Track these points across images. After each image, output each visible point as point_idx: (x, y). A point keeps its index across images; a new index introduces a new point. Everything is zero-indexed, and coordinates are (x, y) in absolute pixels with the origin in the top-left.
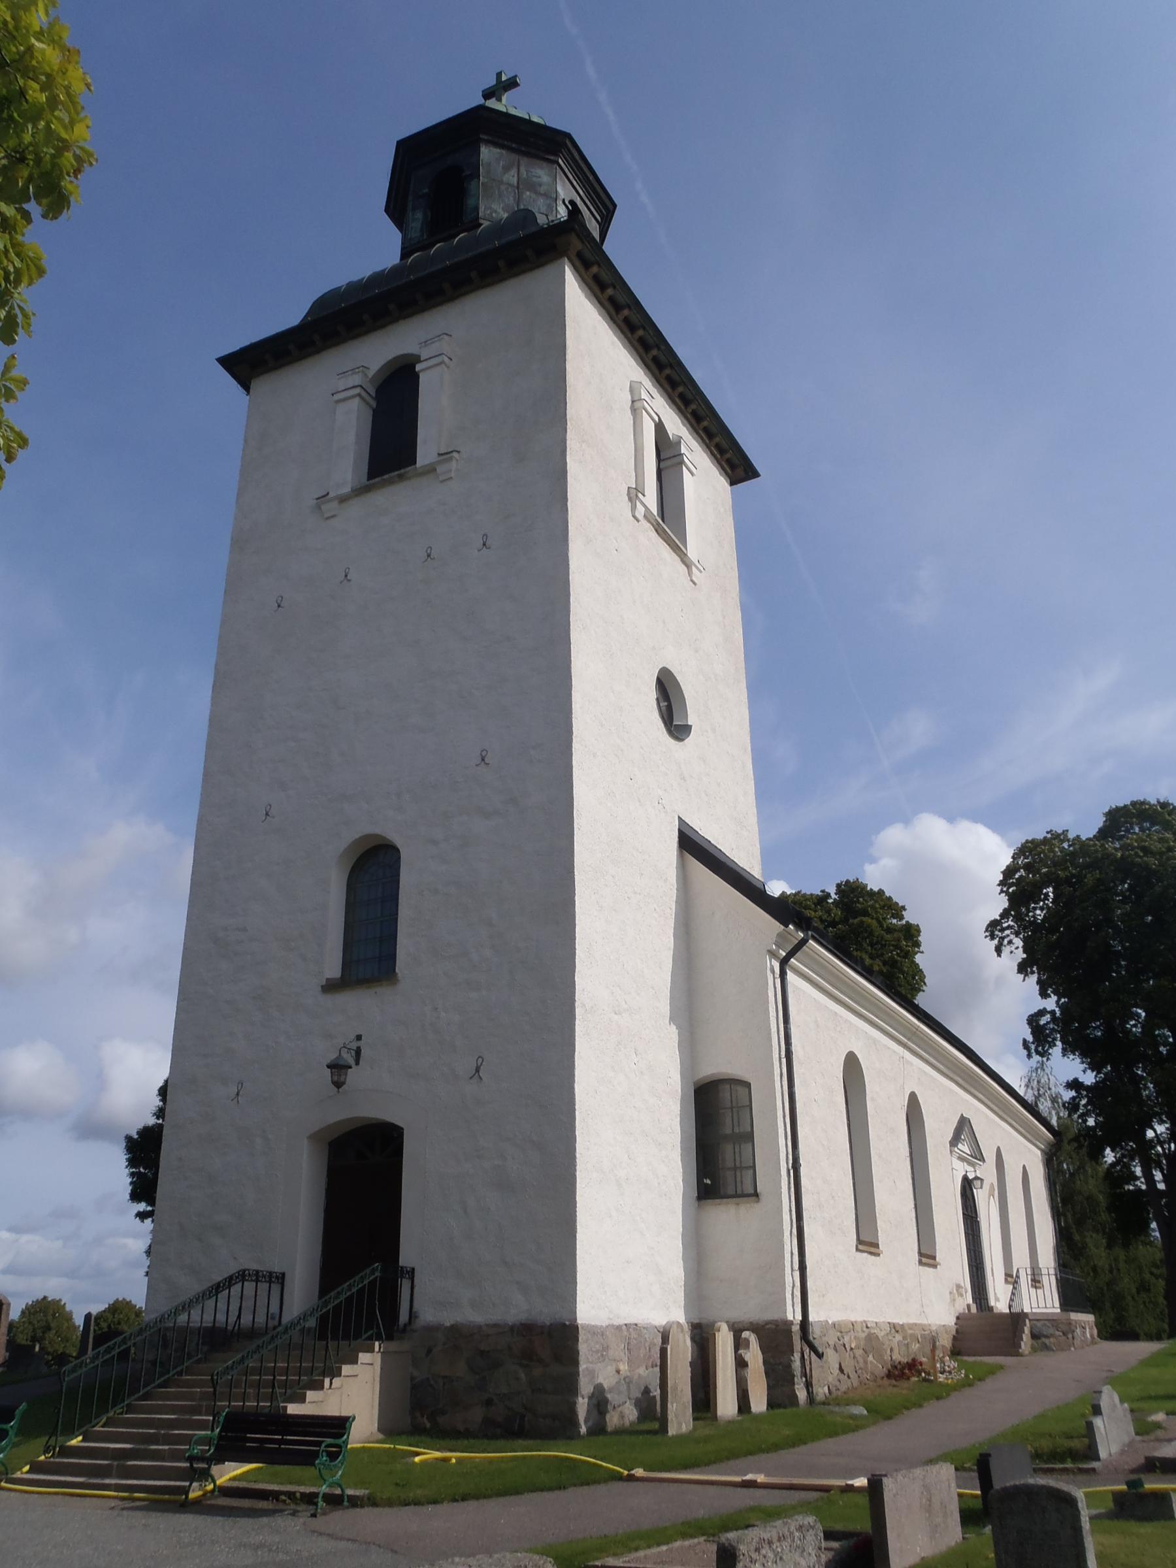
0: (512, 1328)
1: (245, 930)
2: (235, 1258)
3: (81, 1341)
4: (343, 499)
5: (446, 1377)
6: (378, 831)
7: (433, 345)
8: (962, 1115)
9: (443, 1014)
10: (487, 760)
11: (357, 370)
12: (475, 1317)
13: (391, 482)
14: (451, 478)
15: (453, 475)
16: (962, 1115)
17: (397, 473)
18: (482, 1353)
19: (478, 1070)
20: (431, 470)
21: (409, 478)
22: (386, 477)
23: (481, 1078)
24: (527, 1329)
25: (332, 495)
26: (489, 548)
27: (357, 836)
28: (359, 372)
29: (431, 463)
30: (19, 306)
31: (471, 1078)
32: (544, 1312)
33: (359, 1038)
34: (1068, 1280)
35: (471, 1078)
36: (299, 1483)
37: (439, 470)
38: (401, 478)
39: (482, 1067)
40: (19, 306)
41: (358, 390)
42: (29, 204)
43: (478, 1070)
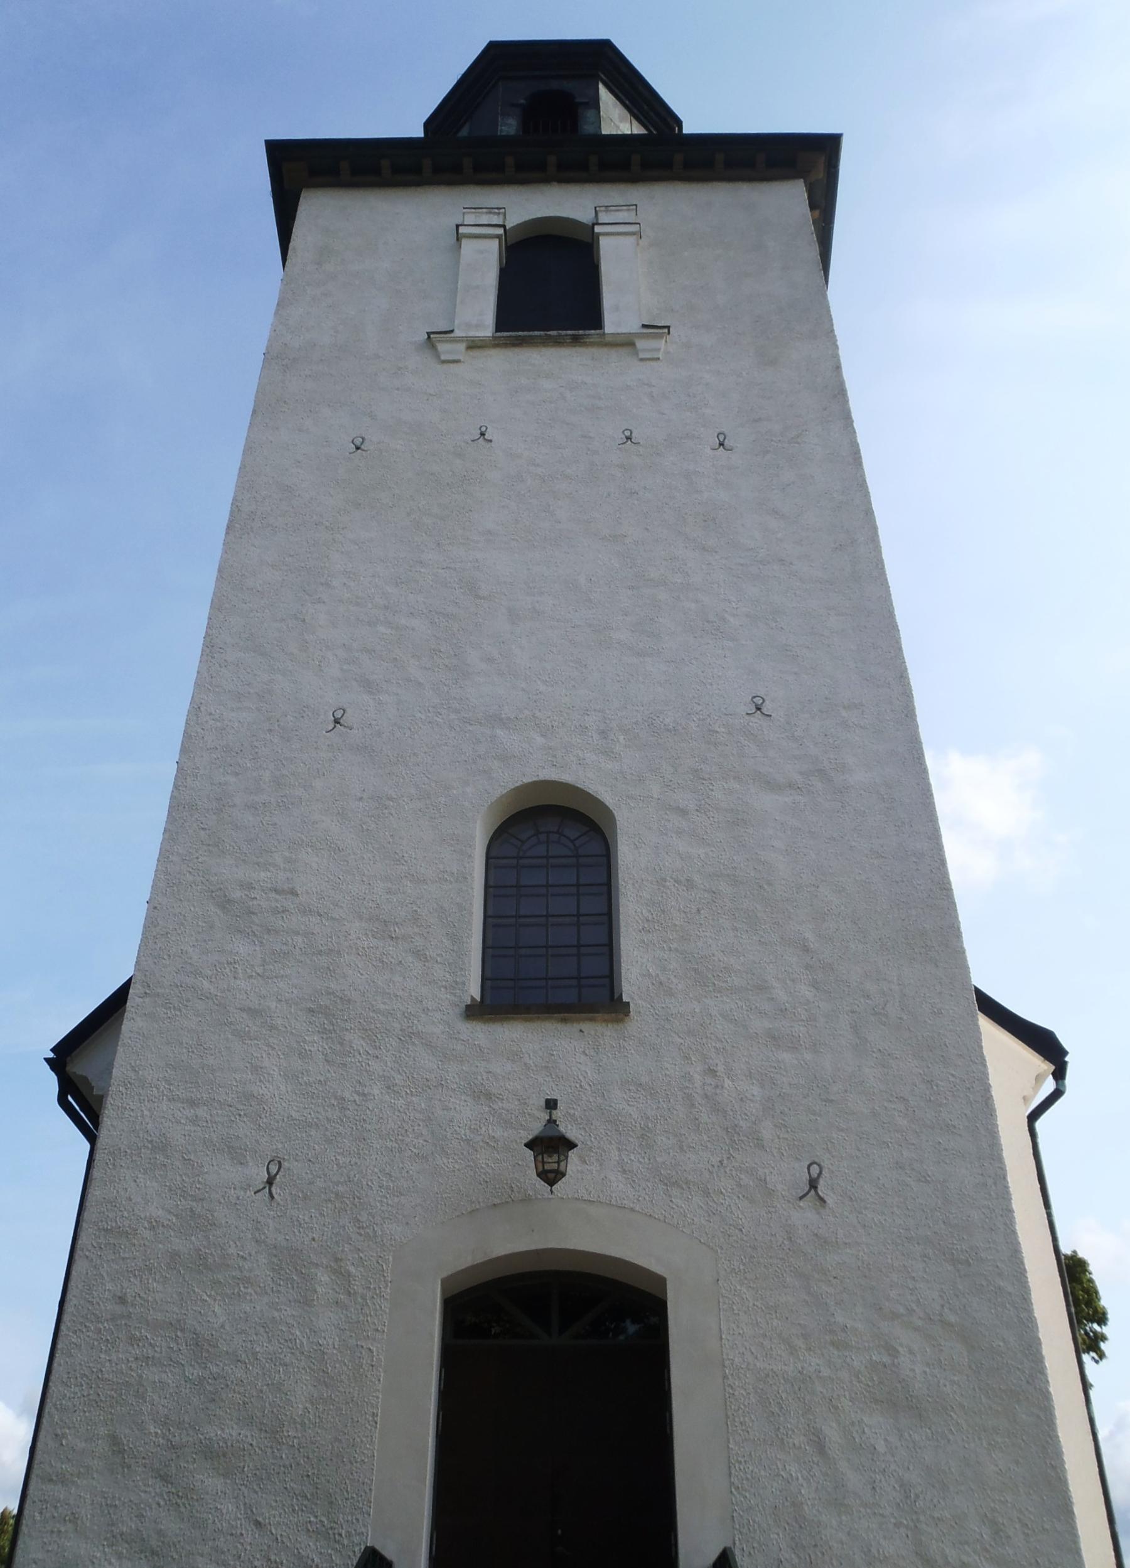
2: (258, 1524)
4: (474, 345)
7: (617, 213)
8: (475, 1012)
9: (728, 1083)
10: (764, 710)
11: (496, 211)
13: (558, 342)
14: (659, 359)
16: (475, 1012)
19: (813, 1184)
20: (626, 343)
21: (585, 345)
22: (553, 333)
25: (458, 333)
28: (499, 213)
31: (801, 1198)
33: (551, 1104)
34: (1099, 1324)
35: (801, 1198)
38: (576, 341)
39: (821, 1182)
41: (501, 231)
43: (813, 1184)
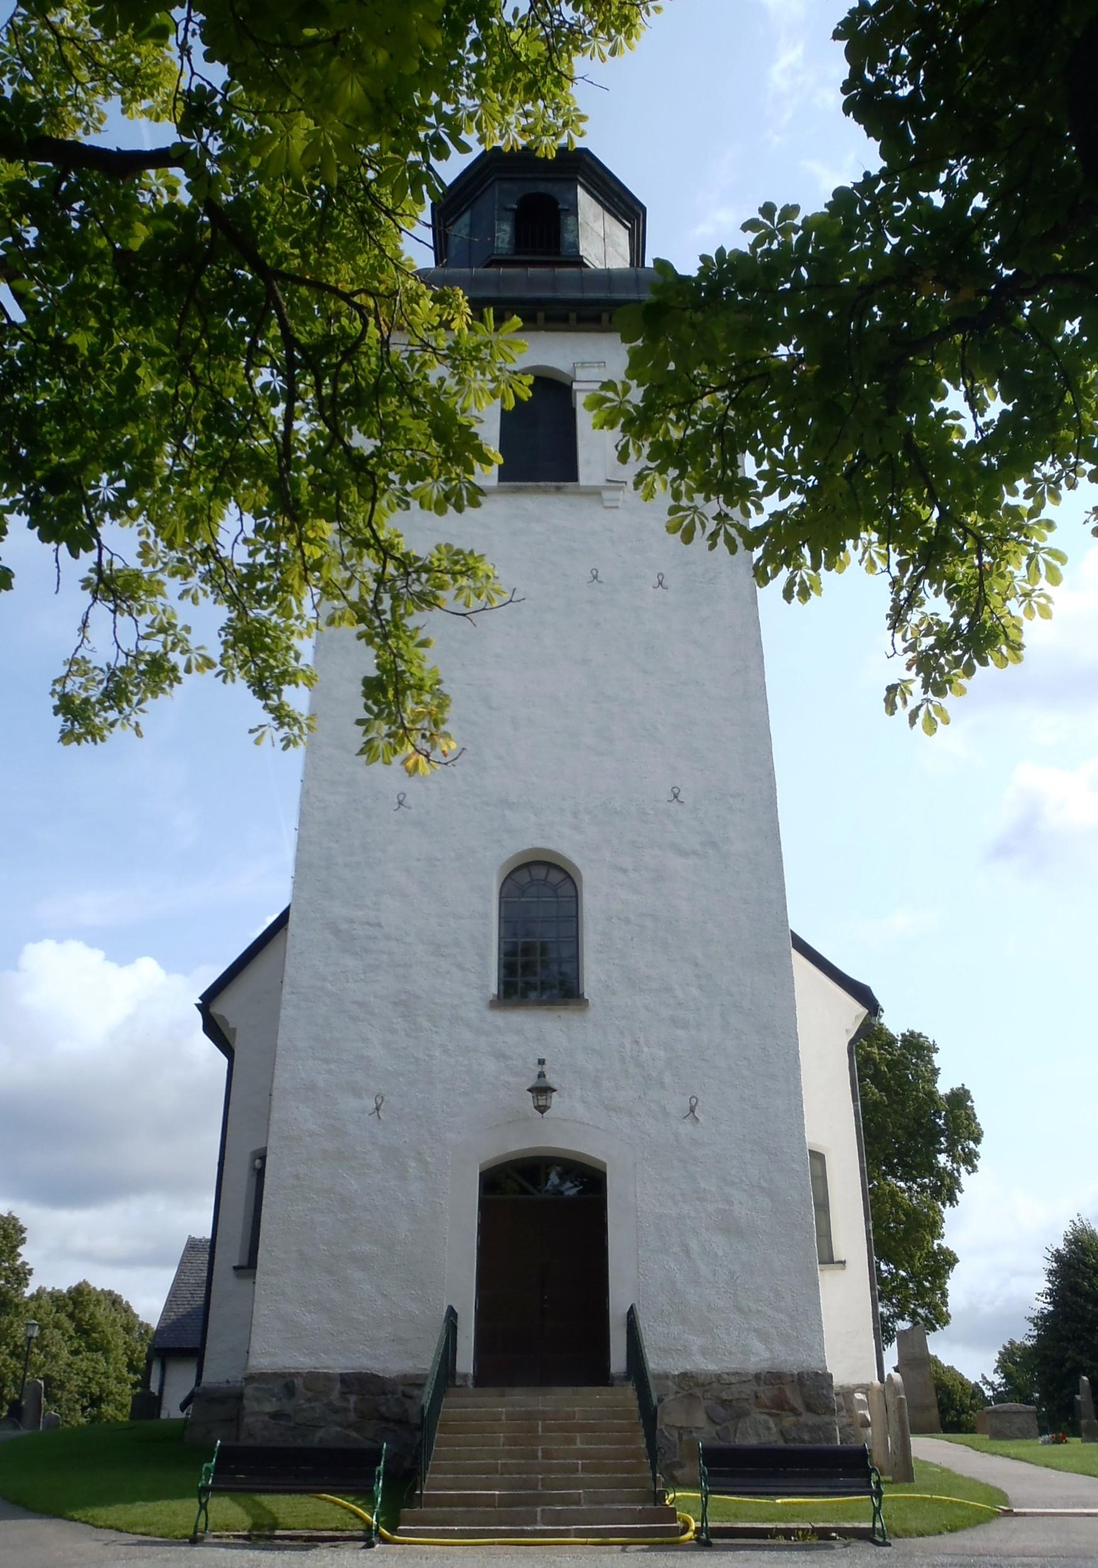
0: (757, 1377)
1: (379, 925)
3: (76, 144)
5: (682, 1428)
6: (551, 846)
9: (645, 1049)
12: (709, 1366)
13: (545, 491)
15: (619, 504)
17: (554, 484)
18: (724, 1403)
19: (692, 1110)
20: (594, 493)
22: (542, 484)
23: (697, 1119)
24: (774, 1378)
26: (666, 588)
27: (525, 847)
29: (596, 487)
30: (263, 733)
32: (791, 1361)
36: (484, 1512)
37: (606, 495)
40: (263, 733)
42: (79, 345)
